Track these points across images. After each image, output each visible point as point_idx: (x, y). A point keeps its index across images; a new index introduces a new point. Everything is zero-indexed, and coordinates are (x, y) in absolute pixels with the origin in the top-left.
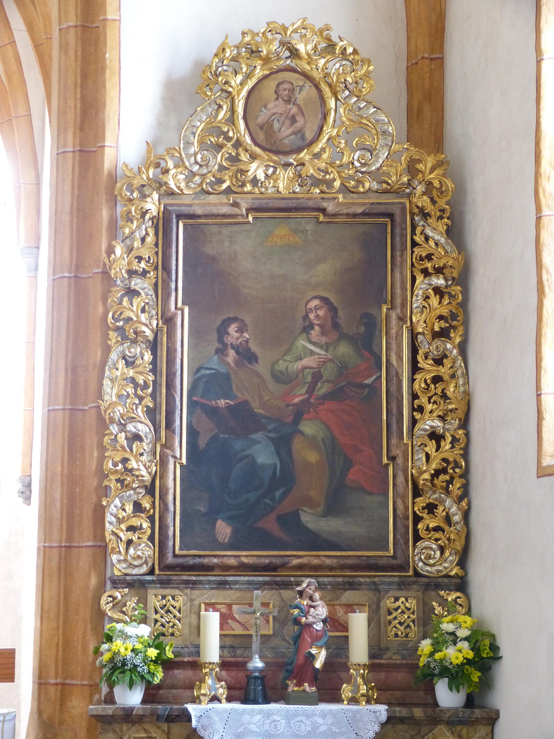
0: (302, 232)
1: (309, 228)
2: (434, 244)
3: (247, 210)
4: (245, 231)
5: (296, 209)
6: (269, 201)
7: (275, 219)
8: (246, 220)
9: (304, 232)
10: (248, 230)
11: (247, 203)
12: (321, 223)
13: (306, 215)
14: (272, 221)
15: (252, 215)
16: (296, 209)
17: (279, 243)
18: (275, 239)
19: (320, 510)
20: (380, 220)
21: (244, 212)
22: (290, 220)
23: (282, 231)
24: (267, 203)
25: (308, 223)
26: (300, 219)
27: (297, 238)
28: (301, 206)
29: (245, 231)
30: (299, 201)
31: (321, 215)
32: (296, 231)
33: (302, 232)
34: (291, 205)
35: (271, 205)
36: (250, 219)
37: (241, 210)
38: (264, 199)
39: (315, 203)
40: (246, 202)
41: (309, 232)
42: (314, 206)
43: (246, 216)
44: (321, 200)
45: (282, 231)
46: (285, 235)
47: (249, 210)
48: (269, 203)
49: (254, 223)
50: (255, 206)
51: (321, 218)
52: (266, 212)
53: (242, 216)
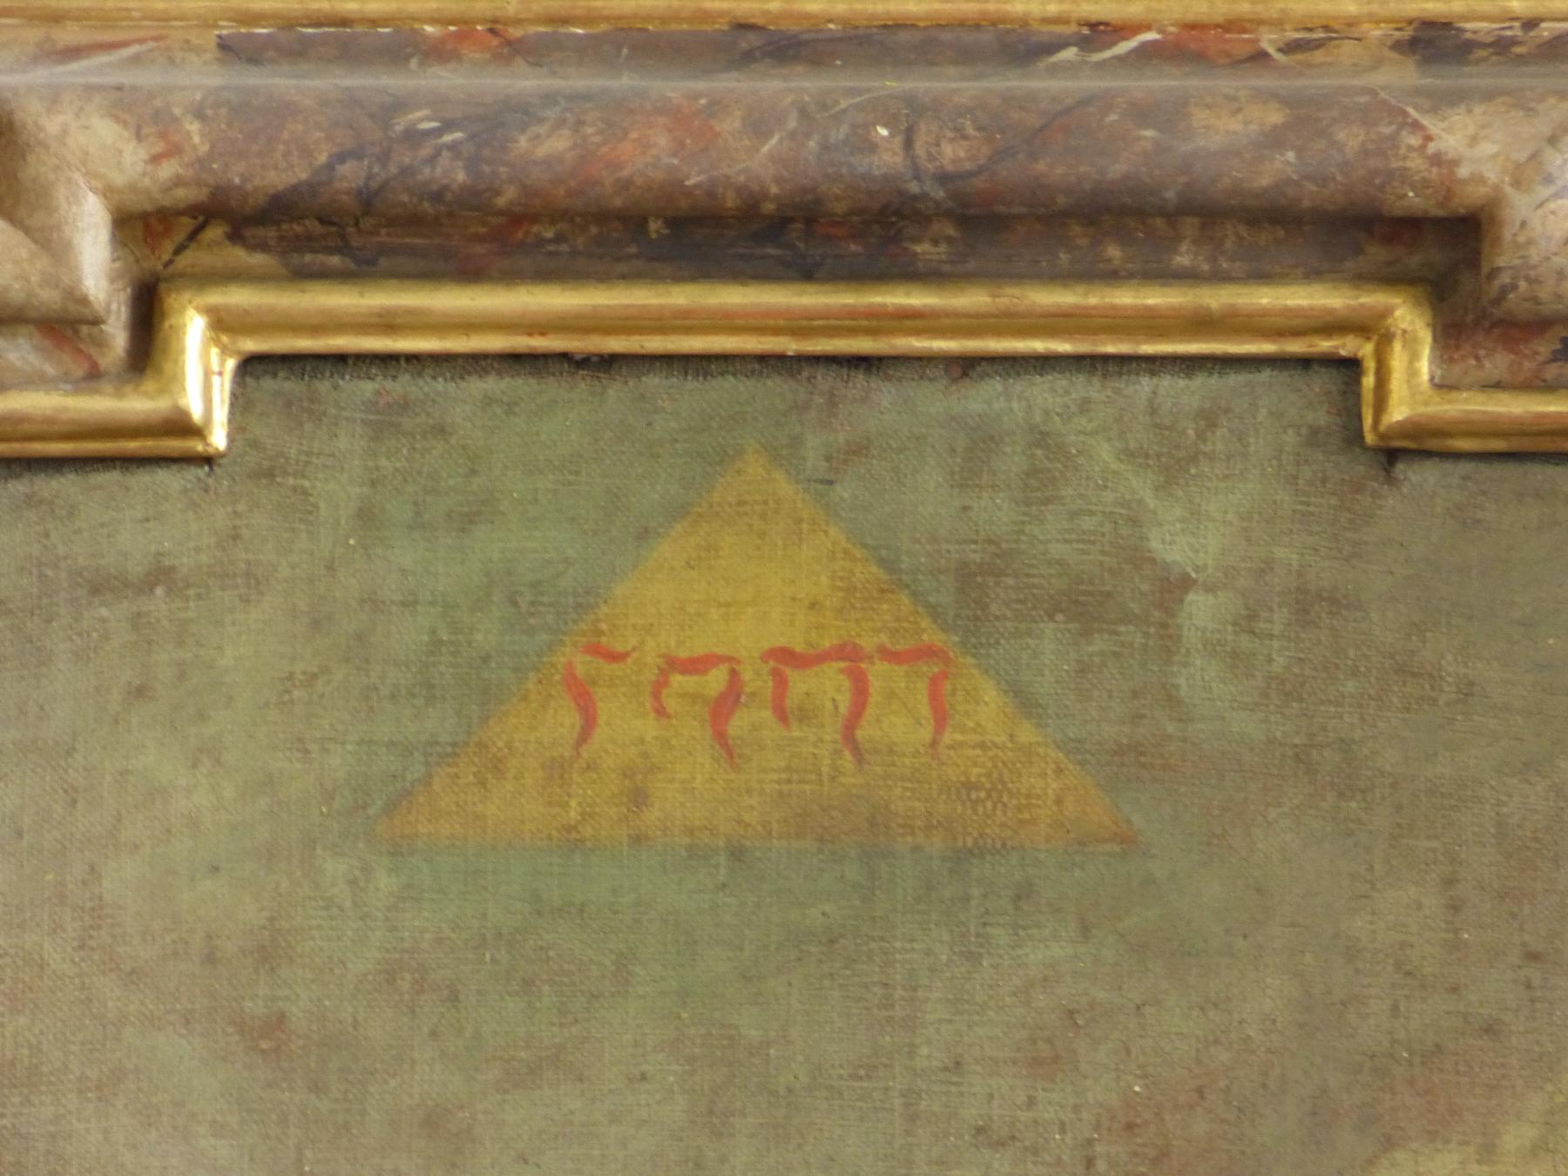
0: (1082, 606)
1: (1196, 535)
2: (317, 223)
3: (138, 225)
4: (101, 586)
5: (992, 224)
6: (524, 81)
7: (616, 391)
8: (137, 404)
9: (1120, 602)
10: (160, 575)
11: (142, 114)
12: (1396, 453)
13: (1153, 323)
14: (568, 415)
15: (223, 324)
16: (992, 224)
17: (692, 786)
18: (624, 723)
19: (208, 56)
20: (1265, 298)
21: (96, 265)
22: (882, 406)
23: (735, 590)
24: (492, 123)
25: (1174, 464)
26: (1044, 392)
27: (985, 708)
28: (1056, 169)
29: (101, 586)
30: (1045, 84)
31: (1408, 317)
32: (975, 597)
33: (1082, 606)
34: (885, 154)
35: (546, 148)
36: (201, 374)
37: (52, 243)
38: (438, 53)
39: (1306, 116)
40: (125, 105)
41: (1200, 612)
42: (1279, 167)
43: (118, 335)
44: (1401, 75)
45: (740, 580)
46: (785, 658)
47: (170, 238)
48: (522, 112)
49: (254, 464)
50: (279, 173)
51: (1412, 376)
52: (470, 274)
53: (65, 327)
